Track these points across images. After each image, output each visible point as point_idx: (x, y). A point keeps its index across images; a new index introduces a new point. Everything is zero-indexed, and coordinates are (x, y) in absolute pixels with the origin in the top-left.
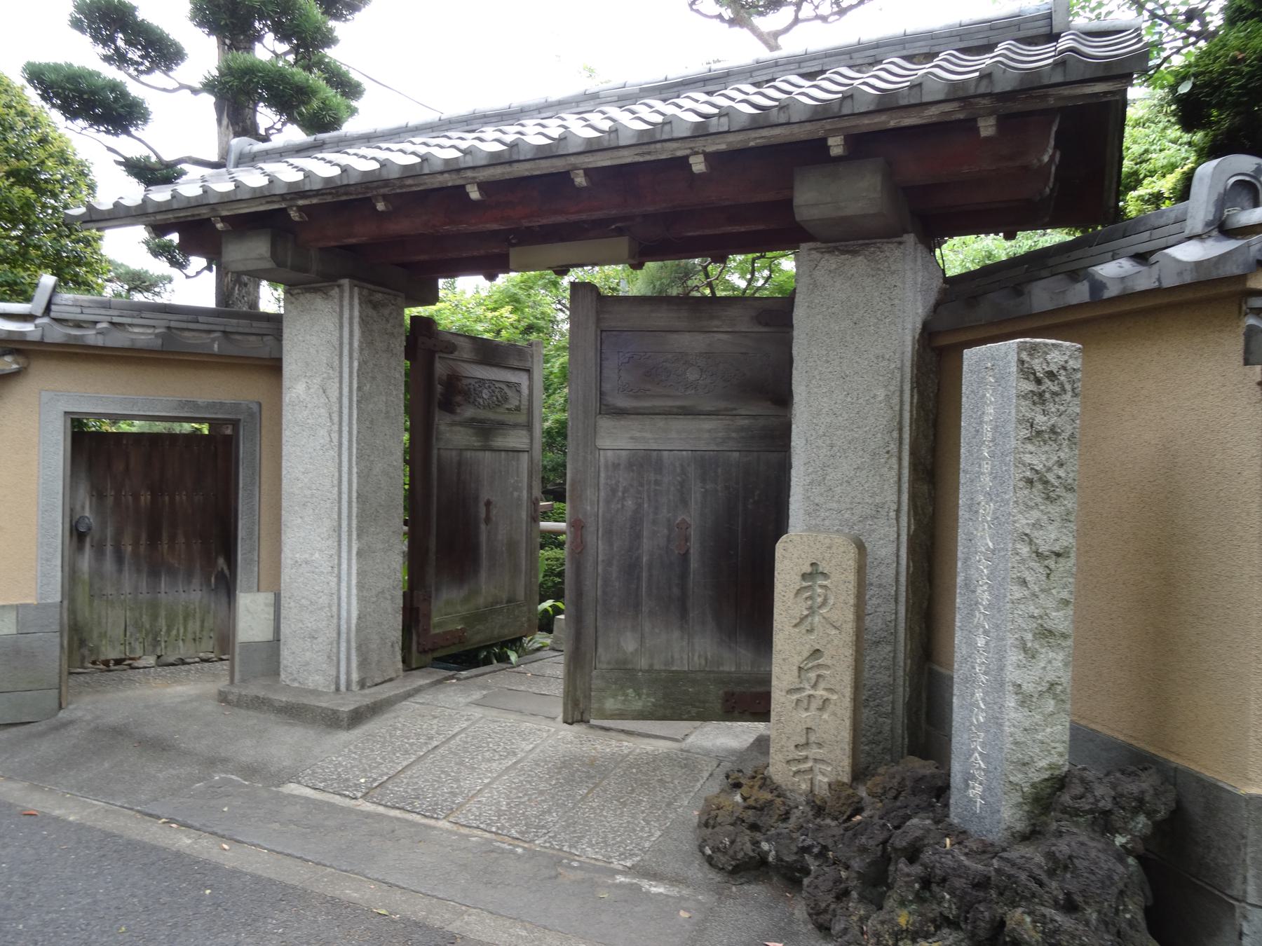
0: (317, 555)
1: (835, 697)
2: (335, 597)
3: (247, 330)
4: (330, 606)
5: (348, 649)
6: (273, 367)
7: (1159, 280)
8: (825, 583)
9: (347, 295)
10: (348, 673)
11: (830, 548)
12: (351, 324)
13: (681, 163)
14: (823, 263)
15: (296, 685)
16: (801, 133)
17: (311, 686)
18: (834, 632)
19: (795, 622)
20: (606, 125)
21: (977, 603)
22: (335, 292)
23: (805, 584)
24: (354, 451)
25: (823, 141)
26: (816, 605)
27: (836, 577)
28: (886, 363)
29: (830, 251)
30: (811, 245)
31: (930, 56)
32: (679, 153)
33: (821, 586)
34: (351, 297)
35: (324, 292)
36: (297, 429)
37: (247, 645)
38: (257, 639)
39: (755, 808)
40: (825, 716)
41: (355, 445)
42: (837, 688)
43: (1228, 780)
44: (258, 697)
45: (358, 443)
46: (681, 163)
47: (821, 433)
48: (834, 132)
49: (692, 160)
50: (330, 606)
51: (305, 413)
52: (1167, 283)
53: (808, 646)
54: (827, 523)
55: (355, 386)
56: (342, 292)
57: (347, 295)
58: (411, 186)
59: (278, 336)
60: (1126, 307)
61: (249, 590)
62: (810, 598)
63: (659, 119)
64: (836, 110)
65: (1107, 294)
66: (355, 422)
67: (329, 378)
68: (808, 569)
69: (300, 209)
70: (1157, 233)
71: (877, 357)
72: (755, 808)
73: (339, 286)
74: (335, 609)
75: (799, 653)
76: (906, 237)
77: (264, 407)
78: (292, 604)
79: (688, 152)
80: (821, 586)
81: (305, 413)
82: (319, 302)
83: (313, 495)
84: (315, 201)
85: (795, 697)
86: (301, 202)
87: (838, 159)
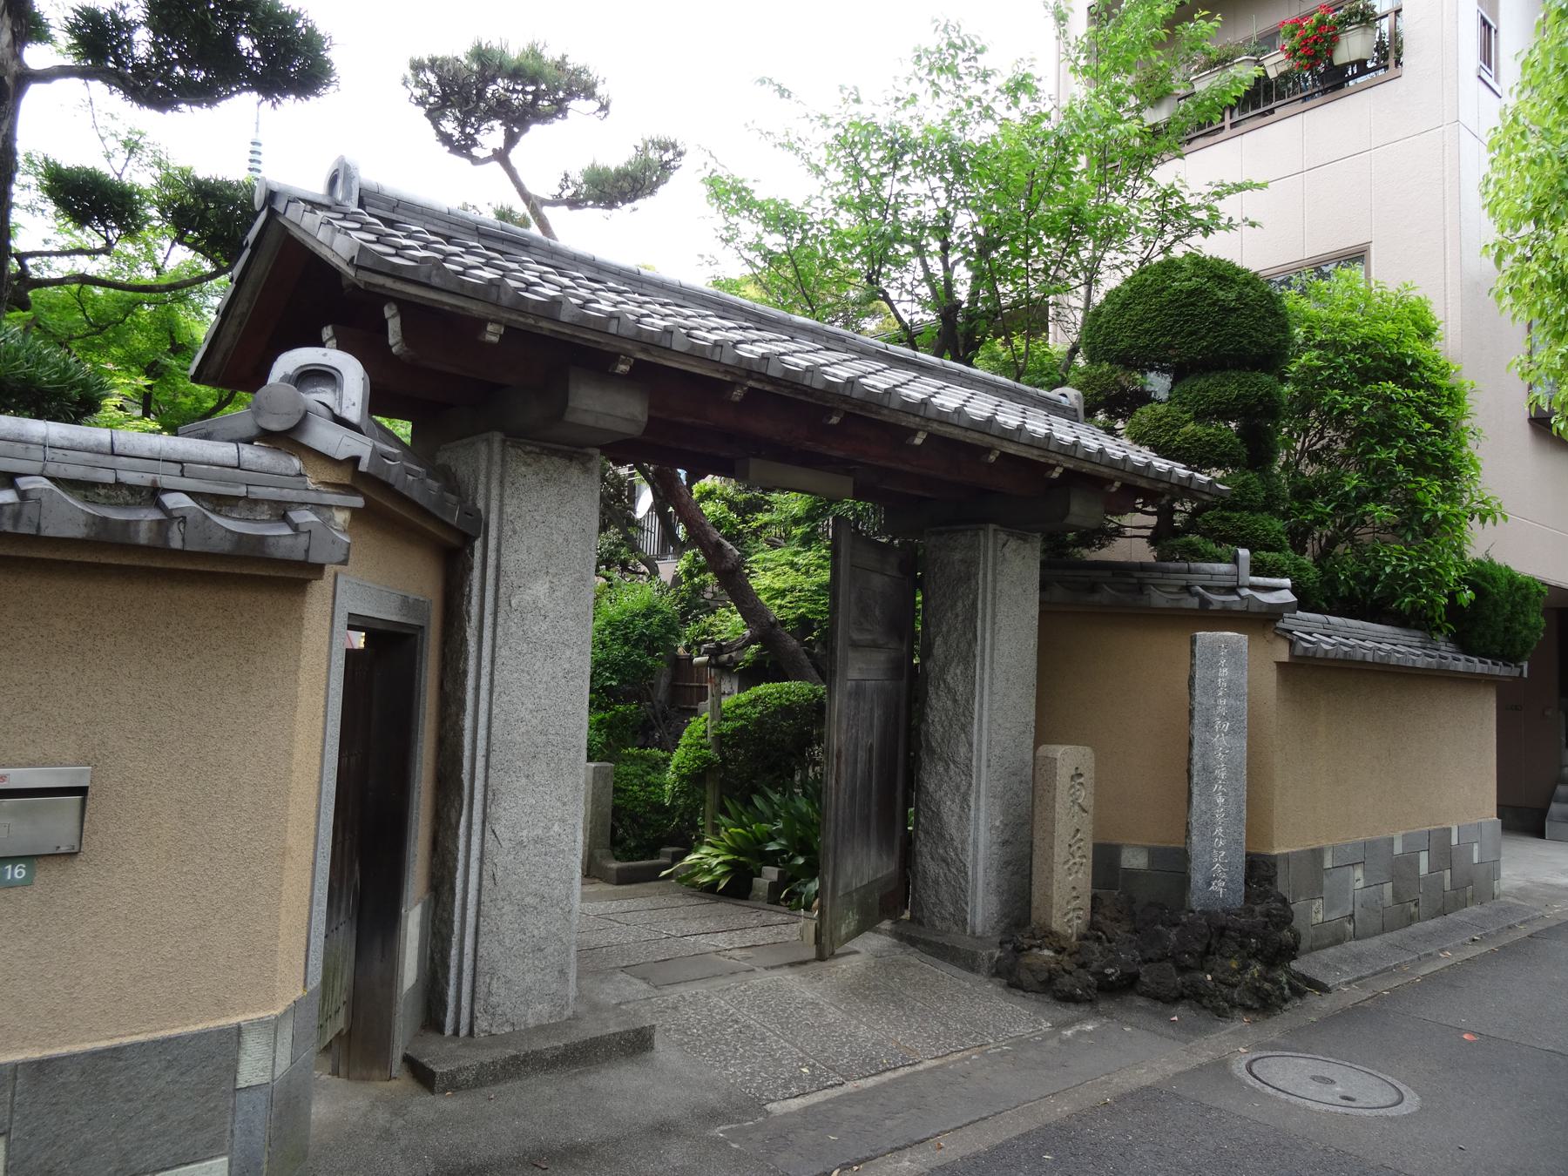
0: (556, 828)
15: (508, 1029)
17: (532, 1022)
36: (524, 647)
43: (1264, 851)
44: (516, 1057)
60: (158, 563)
78: (507, 908)
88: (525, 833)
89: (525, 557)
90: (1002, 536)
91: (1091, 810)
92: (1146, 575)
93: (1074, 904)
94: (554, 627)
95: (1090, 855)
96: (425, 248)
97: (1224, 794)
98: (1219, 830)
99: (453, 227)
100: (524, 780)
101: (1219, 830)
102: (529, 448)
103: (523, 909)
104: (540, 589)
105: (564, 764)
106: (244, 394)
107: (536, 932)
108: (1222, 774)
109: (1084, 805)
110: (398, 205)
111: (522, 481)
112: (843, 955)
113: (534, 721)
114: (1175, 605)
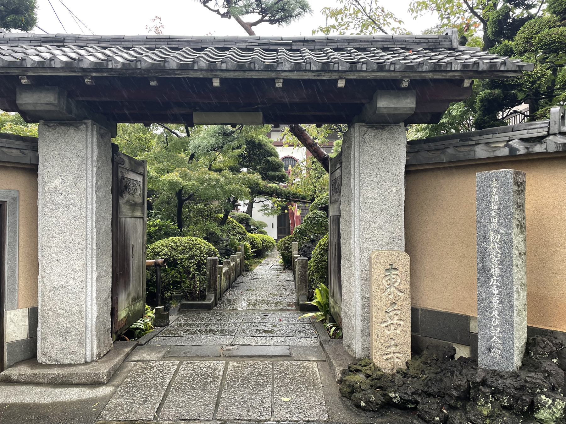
0: (71, 282)
1: (402, 323)
2: (84, 306)
3: (12, 146)
4: (80, 312)
5: (92, 336)
6: (31, 170)
7: (546, 149)
8: (396, 272)
9: (90, 129)
10: (92, 350)
11: (398, 257)
12: (92, 145)
13: (146, 80)
14: (368, 132)
16: (201, 75)
18: (400, 294)
19: (383, 291)
20: (48, 56)
21: (491, 275)
22: (83, 127)
23: (387, 274)
24: (94, 219)
25: (211, 80)
26: (392, 283)
27: (401, 269)
28: (396, 177)
29: (372, 127)
30: (361, 124)
31: (202, 49)
32: (333, 77)
33: (394, 274)
34: (92, 130)
35: (77, 128)
36: (53, 207)
37: (13, 345)
38: (18, 339)
39: (376, 379)
40: (398, 332)
41: (95, 216)
42: (404, 319)
45: (96, 215)
46: (146, 80)
47: (368, 207)
48: (216, 77)
49: (214, 80)
50: (80, 312)
51: (61, 198)
52: (549, 150)
53: (389, 302)
54: (371, 246)
55: (95, 182)
56: (87, 127)
57: (90, 129)
58: (178, 74)
59: (35, 149)
60: (546, 156)
61: (12, 308)
62: (389, 280)
63: (104, 58)
64: (19, 64)
65: (518, 153)
66: (94, 202)
67: (79, 177)
68: (389, 267)
69: (93, 78)
70: (494, 136)
71: (393, 174)
72: (376, 379)
73: (85, 123)
74: (84, 313)
75: (386, 306)
76: (401, 124)
77: (21, 194)
78: (50, 313)
79: (337, 77)
80: (394, 274)
81: (61, 198)
82: (72, 132)
83: (66, 246)
84: (105, 74)
85: (384, 325)
86: (94, 74)
87: (404, 89)
88: (56, 283)
89: (51, 169)
90: (364, 129)
91: (408, 291)
92: (482, 137)
93: (393, 349)
94: (66, 198)
95: (409, 320)
96: (424, 56)
97: (497, 287)
98: (495, 313)
99: (223, 46)
100: (56, 262)
101: (495, 313)
102: (52, 125)
103: (58, 315)
104: (57, 182)
105: (75, 255)
106: (262, 115)
107: (65, 325)
108: (495, 271)
109: (401, 287)
110: (225, 41)
111: (48, 139)
112: (367, 333)
113: (61, 238)
114: (492, 155)
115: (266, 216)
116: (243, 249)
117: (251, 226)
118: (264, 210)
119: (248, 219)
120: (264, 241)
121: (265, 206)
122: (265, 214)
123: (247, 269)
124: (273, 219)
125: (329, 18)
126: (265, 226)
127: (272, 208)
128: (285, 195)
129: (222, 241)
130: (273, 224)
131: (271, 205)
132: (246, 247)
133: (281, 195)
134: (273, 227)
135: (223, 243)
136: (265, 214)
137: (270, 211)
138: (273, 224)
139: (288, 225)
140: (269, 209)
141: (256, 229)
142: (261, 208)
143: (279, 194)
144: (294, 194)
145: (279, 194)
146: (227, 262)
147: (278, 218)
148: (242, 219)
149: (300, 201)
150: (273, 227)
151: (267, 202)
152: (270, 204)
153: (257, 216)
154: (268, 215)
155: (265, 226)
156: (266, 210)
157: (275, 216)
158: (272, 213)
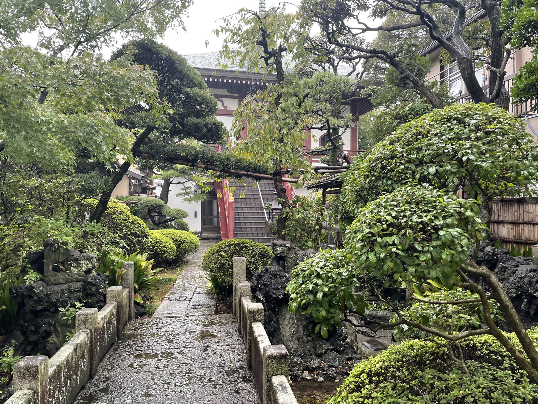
115: (187, 203)
116: (131, 274)
117: (165, 216)
118: (185, 194)
119: (160, 207)
120: (179, 243)
121: (185, 188)
122: (185, 199)
123: (143, 312)
124: (197, 206)
125: (242, 47)
126: (185, 215)
127: (196, 191)
128: (221, 162)
129: (76, 260)
130: (196, 213)
131: (193, 189)
132: (137, 266)
133: (212, 163)
134: (196, 216)
135: (79, 266)
136: (185, 199)
137: (192, 196)
138: (196, 213)
139: (215, 214)
140: (191, 193)
141: (172, 220)
142: (180, 192)
143: (209, 163)
144: (238, 161)
145: (209, 163)
146: (28, 369)
147: (203, 204)
148: (152, 206)
149: (248, 176)
150: (196, 216)
151: (188, 184)
152: (193, 187)
153: (175, 202)
154: (190, 200)
155: (185, 215)
156: (187, 194)
157: (200, 203)
158: (195, 198)
